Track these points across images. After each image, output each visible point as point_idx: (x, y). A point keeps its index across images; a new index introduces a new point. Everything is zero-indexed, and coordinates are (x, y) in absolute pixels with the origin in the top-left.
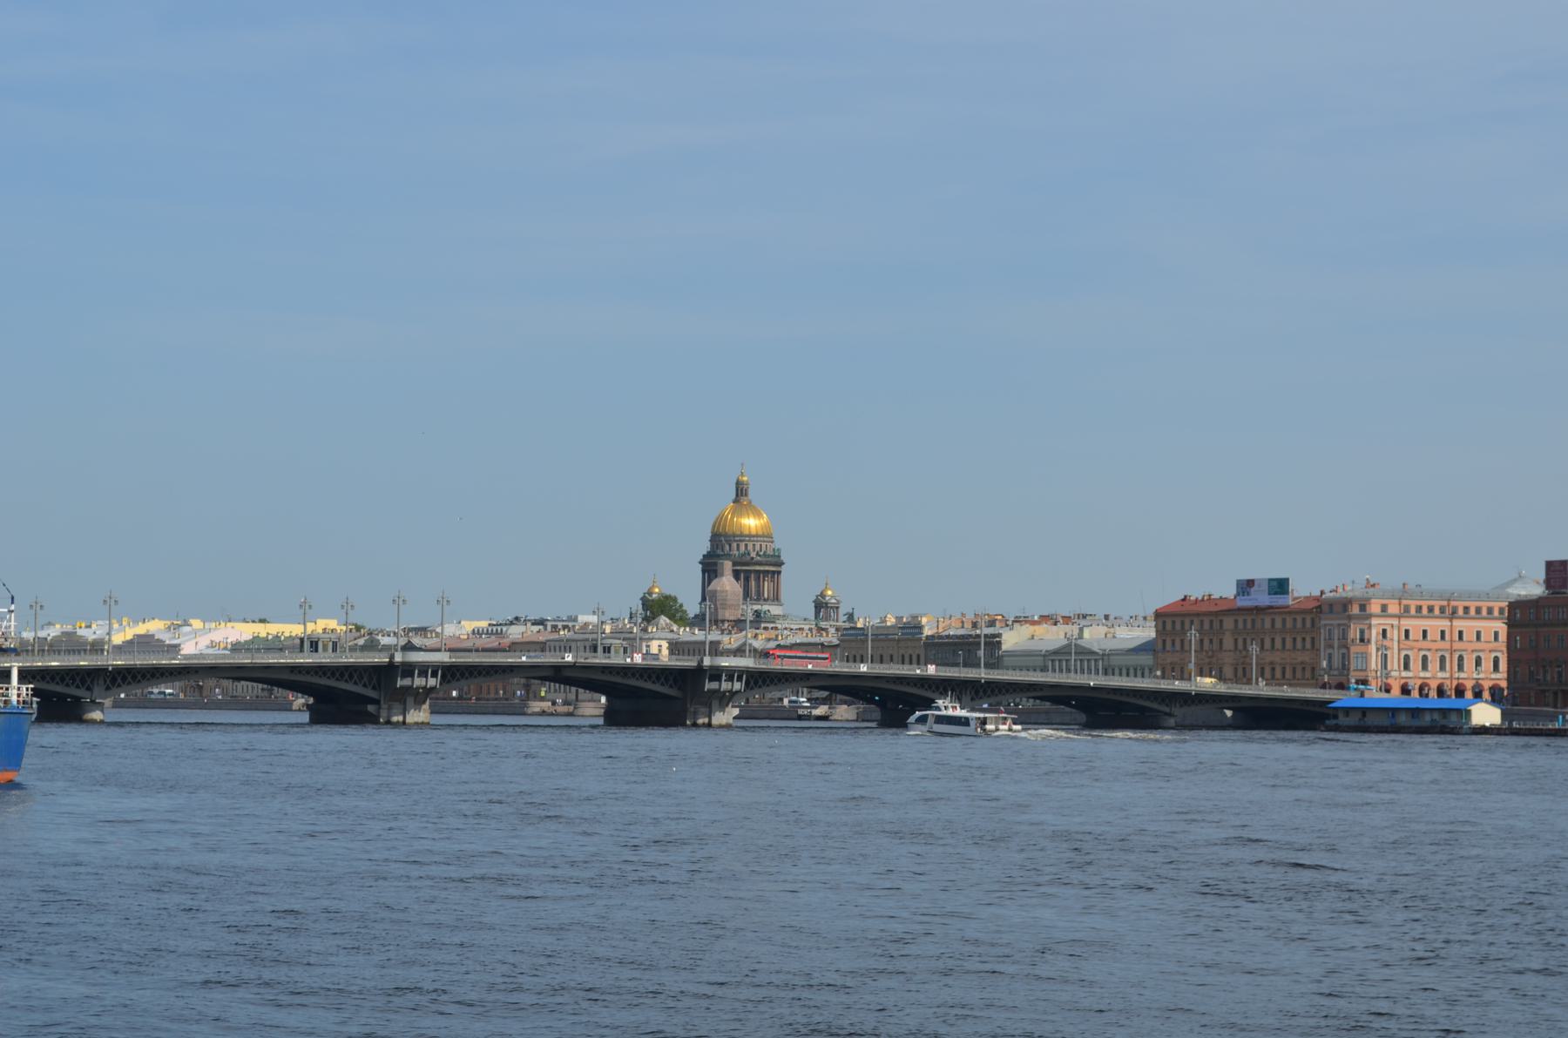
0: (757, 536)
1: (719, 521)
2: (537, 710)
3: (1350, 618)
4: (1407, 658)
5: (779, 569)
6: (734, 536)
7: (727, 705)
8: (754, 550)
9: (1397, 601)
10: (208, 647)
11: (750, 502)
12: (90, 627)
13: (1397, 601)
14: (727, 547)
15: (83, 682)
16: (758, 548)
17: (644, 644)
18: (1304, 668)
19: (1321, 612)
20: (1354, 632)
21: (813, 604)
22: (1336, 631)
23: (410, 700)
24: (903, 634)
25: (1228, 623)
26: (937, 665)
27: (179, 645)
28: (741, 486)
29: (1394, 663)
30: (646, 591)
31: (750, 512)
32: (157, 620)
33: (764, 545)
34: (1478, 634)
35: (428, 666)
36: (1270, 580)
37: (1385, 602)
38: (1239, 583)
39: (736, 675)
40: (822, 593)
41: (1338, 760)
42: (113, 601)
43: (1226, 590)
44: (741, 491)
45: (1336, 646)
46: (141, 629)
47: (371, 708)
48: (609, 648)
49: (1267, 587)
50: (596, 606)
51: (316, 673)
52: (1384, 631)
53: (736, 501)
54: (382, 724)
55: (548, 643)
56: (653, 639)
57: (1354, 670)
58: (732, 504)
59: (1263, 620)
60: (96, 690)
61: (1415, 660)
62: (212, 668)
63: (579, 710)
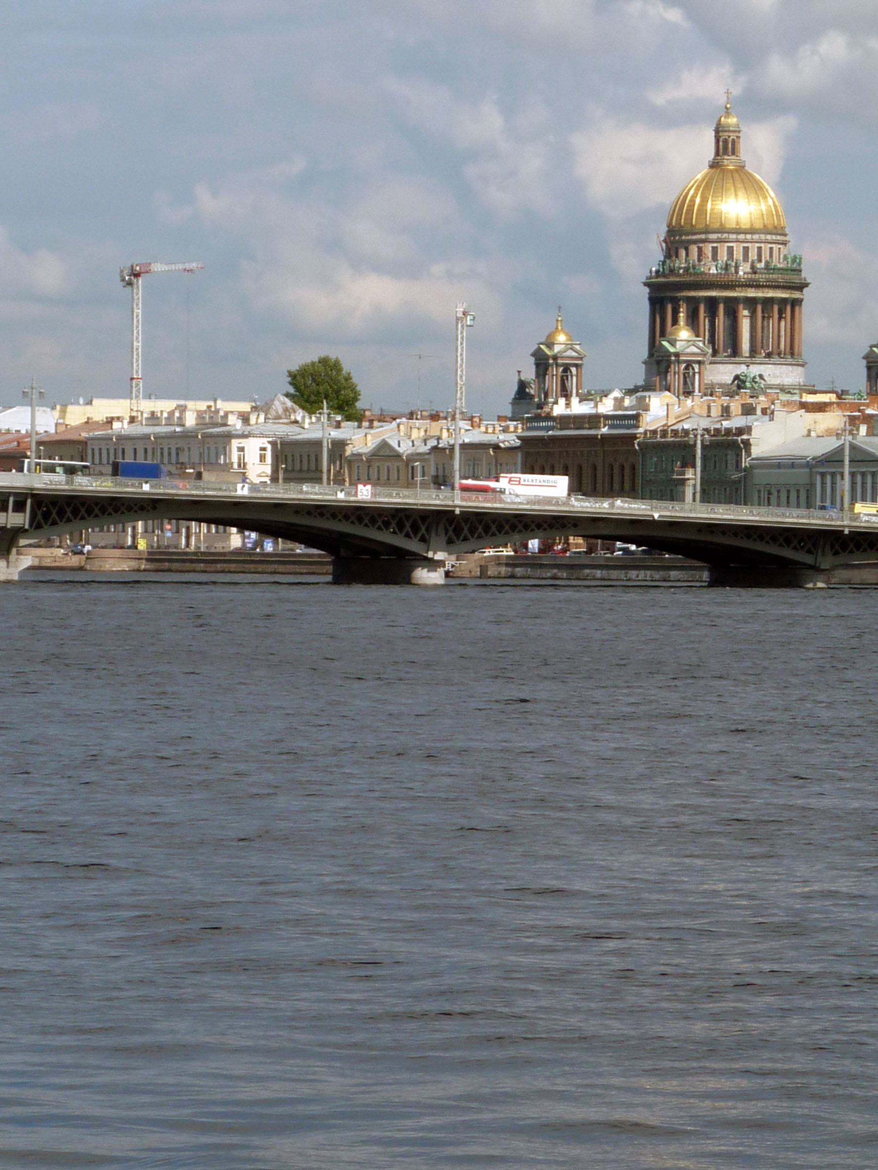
5: (796, 295)
16: (753, 255)
21: (533, 360)
26: (374, 485)
30: (543, 340)
31: (739, 185)
33: (766, 248)
35: (10, 493)
39: (11, 499)
53: (714, 165)
55: (89, 443)
60: (434, 540)
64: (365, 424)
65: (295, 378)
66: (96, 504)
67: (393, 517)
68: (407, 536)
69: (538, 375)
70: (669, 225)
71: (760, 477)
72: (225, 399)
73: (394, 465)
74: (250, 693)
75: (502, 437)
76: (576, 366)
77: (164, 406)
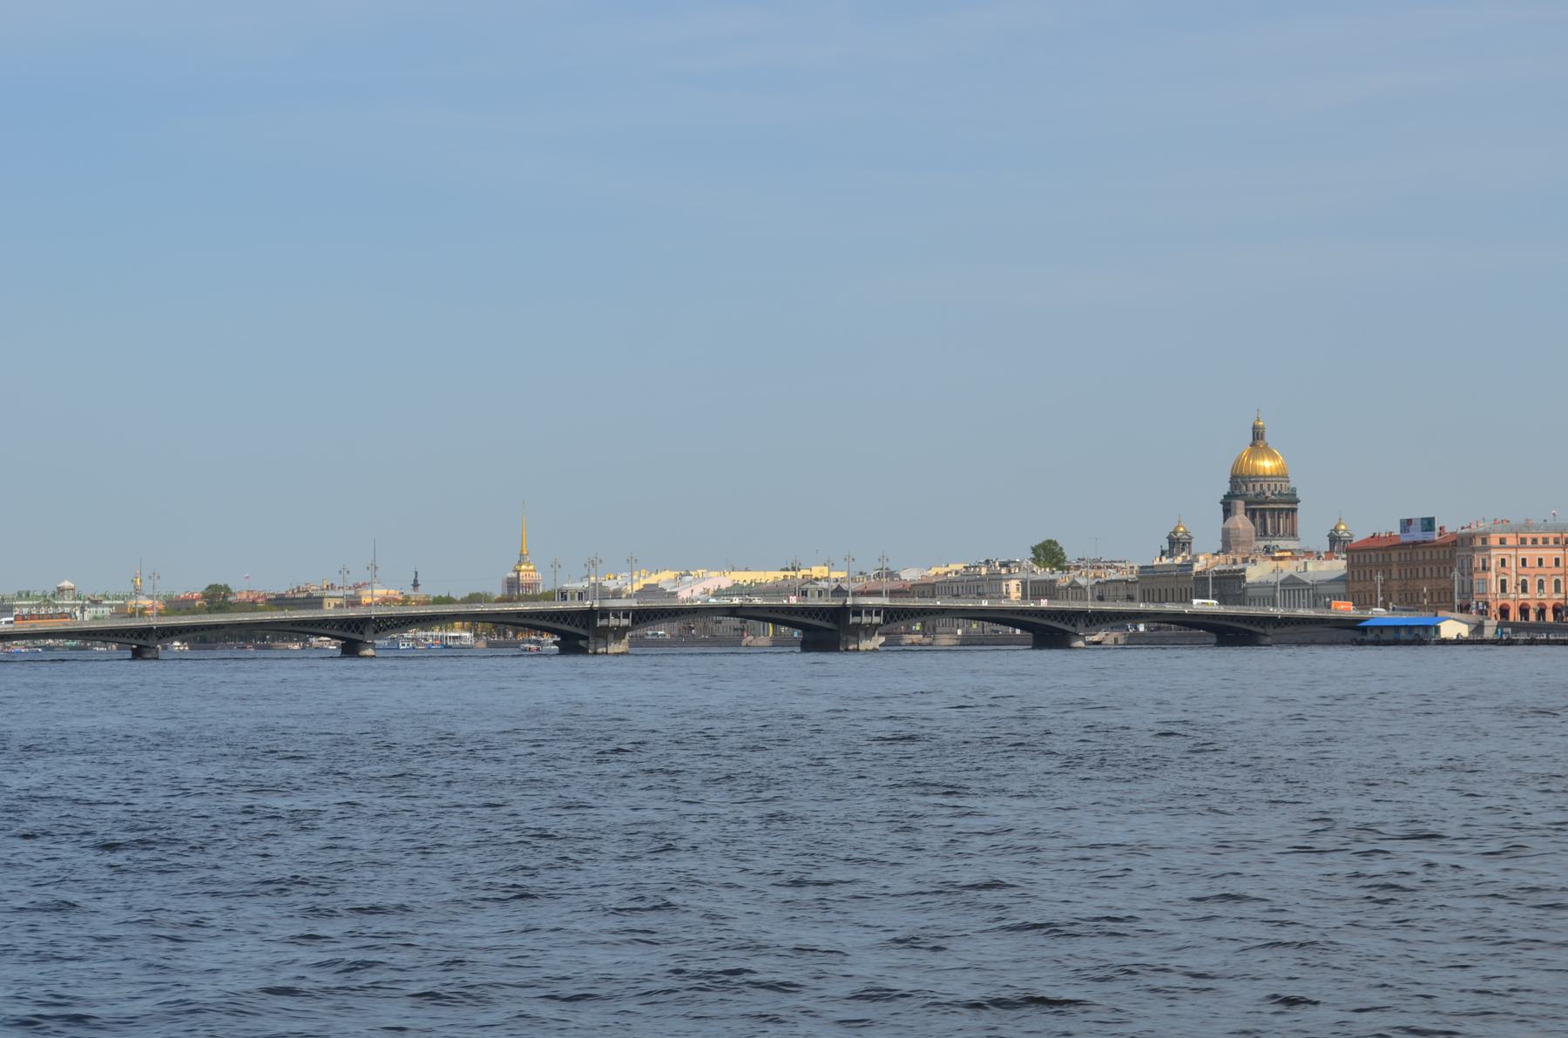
0: (1272, 476)
1: (1239, 460)
2: (910, 641)
3: (1474, 550)
5: (1294, 506)
6: (1250, 477)
7: (874, 635)
8: (1269, 489)
9: (1514, 535)
10: (702, 594)
12: (615, 578)
13: (1514, 535)
14: (1244, 488)
15: (357, 628)
16: (1272, 488)
17: (1004, 584)
18: (1445, 593)
19: (1456, 546)
20: (1477, 563)
21: (1167, 540)
22: (1466, 561)
23: (611, 636)
24: (1180, 570)
25: (1395, 556)
27: (676, 593)
28: (1257, 431)
32: (667, 571)
34: (1540, 561)
36: (1423, 519)
37: (1503, 535)
38: (1402, 522)
40: (1336, 527)
41: (96, 660)
42: (156, 576)
43: (1389, 526)
44: (1257, 434)
45: (1466, 574)
46: (653, 580)
47: (582, 643)
48: (806, 592)
49: (1420, 526)
50: (827, 559)
51: (538, 617)
52: (1503, 561)
53: (1253, 445)
54: (842, 651)
55: (937, 584)
56: (1011, 579)
57: (1477, 594)
58: (1249, 447)
59: (1417, 553)
60: (367, 633)
61: (1531, 585)
62: (455, 615)
63: (937, 641)
66: (895, 612)
67: (345, 622)
68: (1066, 623)
69: (1170, 548)
71: (1251, 592)
73: (1079, 591)
74: (965, 696)
75: (1130, 576)
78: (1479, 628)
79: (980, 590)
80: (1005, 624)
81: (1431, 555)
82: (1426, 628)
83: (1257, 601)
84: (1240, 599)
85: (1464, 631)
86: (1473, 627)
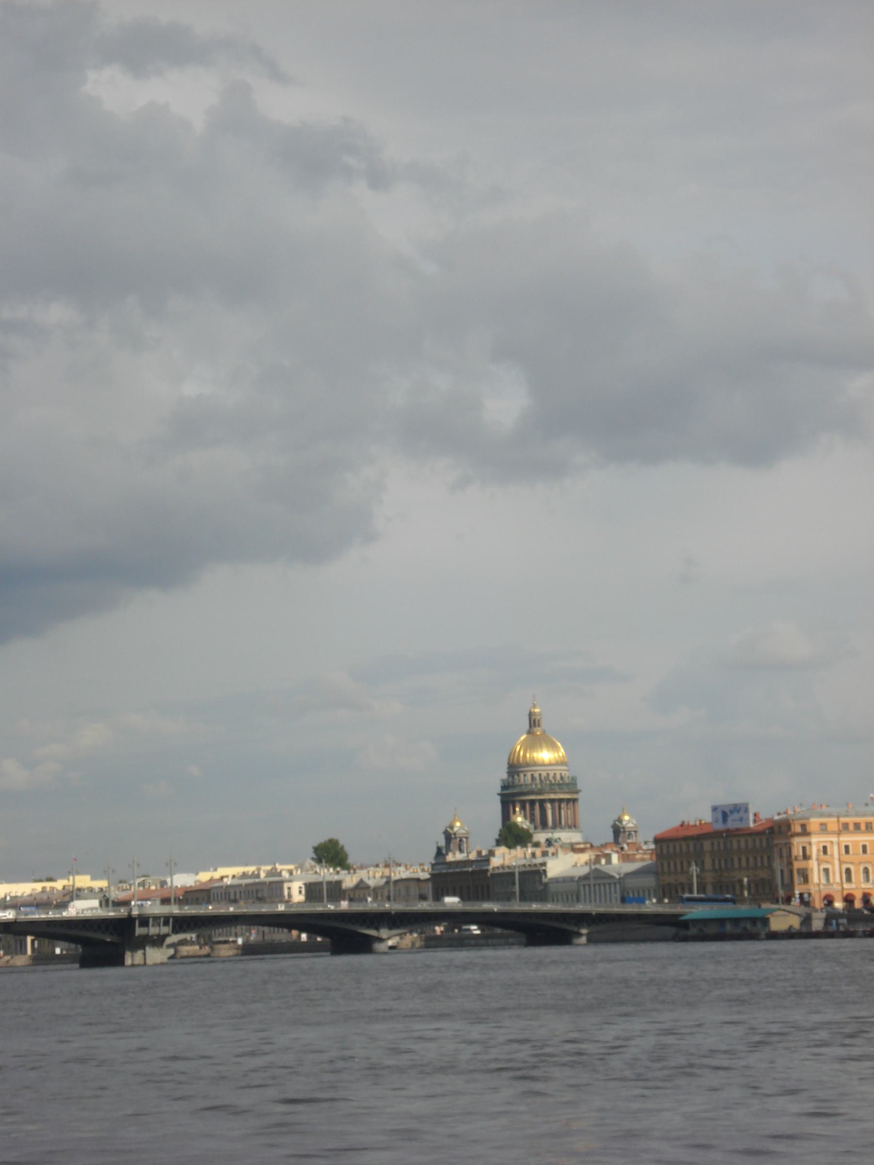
4: (848, 871)
5: (575, 796)
11: (544, 732)
13: (835, 819)
20: (797, 851)
25: (707, 845)
29: (836, 877)
34: (864, 848)
52: (825, 848)
59: (731, 842)
64: (352, 871)
65: (316, 850)
70: (509, 763)
72: (281, 864)
76: (466, 838)
77: (251, 869)
78: (807, 920)
79: (260, 895)
80: (290, 927)
81: (747, 844)
82: (754, 920)
83: (560, 898)
84: (543, 895)
85: (795, 922)
86: (802, 919)
